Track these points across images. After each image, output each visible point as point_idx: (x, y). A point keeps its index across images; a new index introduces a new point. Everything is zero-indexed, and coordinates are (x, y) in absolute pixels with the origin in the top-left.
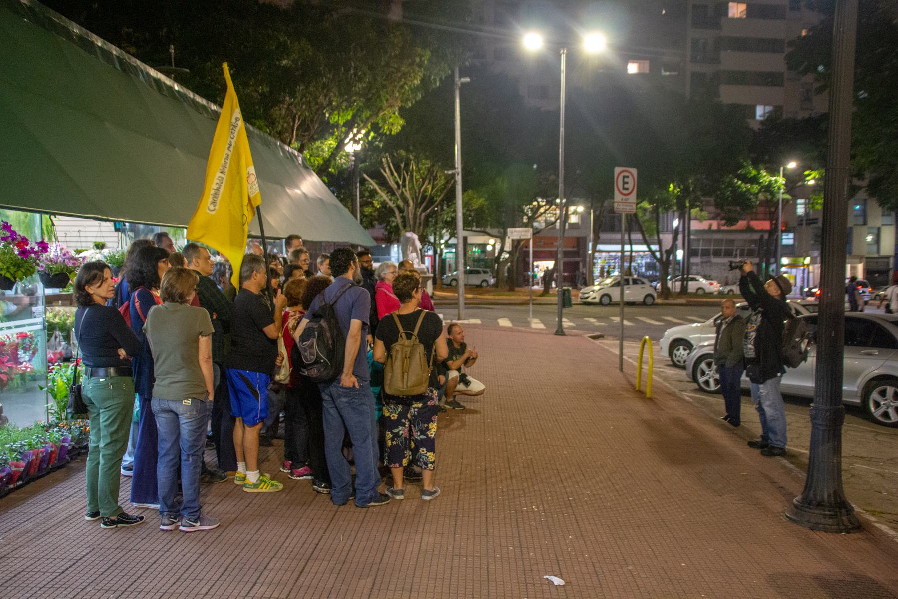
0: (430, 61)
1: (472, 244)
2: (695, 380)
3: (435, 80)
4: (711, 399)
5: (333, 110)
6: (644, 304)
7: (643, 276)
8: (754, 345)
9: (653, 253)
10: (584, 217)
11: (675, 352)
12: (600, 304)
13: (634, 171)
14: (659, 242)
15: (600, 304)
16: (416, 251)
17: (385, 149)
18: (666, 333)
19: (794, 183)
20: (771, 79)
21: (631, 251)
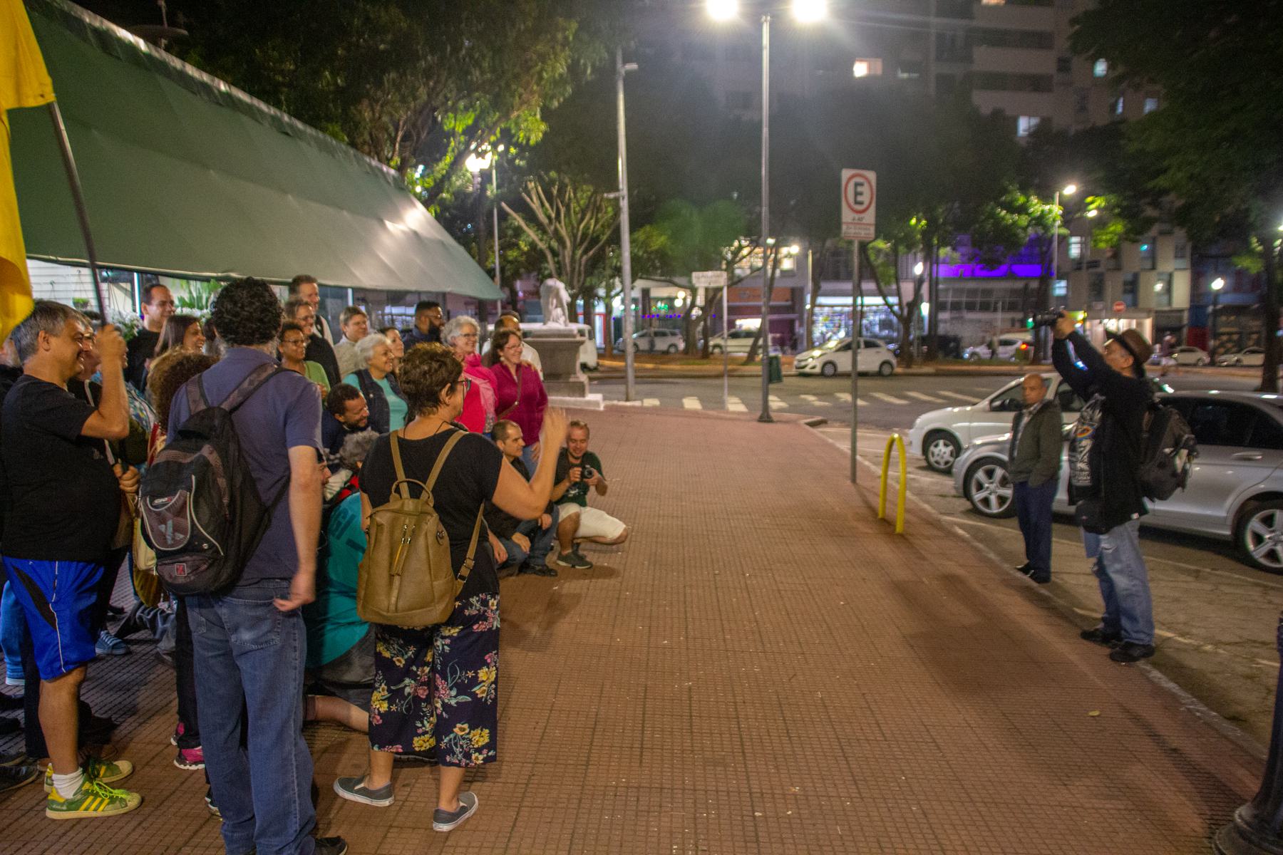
0: (576, 35)
1: (658, 299)
2: (967, 494)
3: (585, 65)
4: (993, 528)
5: (446, 112)
6: (879, 374)
7: (876, 336)
8: (1090, 463)
9: (890, 306)
10: (800, 260)
11: (932, 448)
12: (822, 375)
13: (872, 176)
14: (898, 294)
15: (822, 375)
16: (562, 306)
17: (531, 169)
18: (918, 421)
19: (1072, 211)
20: (1037, 84)
21: (862, 306)
